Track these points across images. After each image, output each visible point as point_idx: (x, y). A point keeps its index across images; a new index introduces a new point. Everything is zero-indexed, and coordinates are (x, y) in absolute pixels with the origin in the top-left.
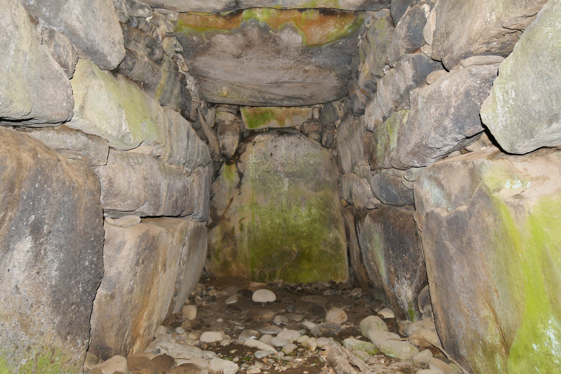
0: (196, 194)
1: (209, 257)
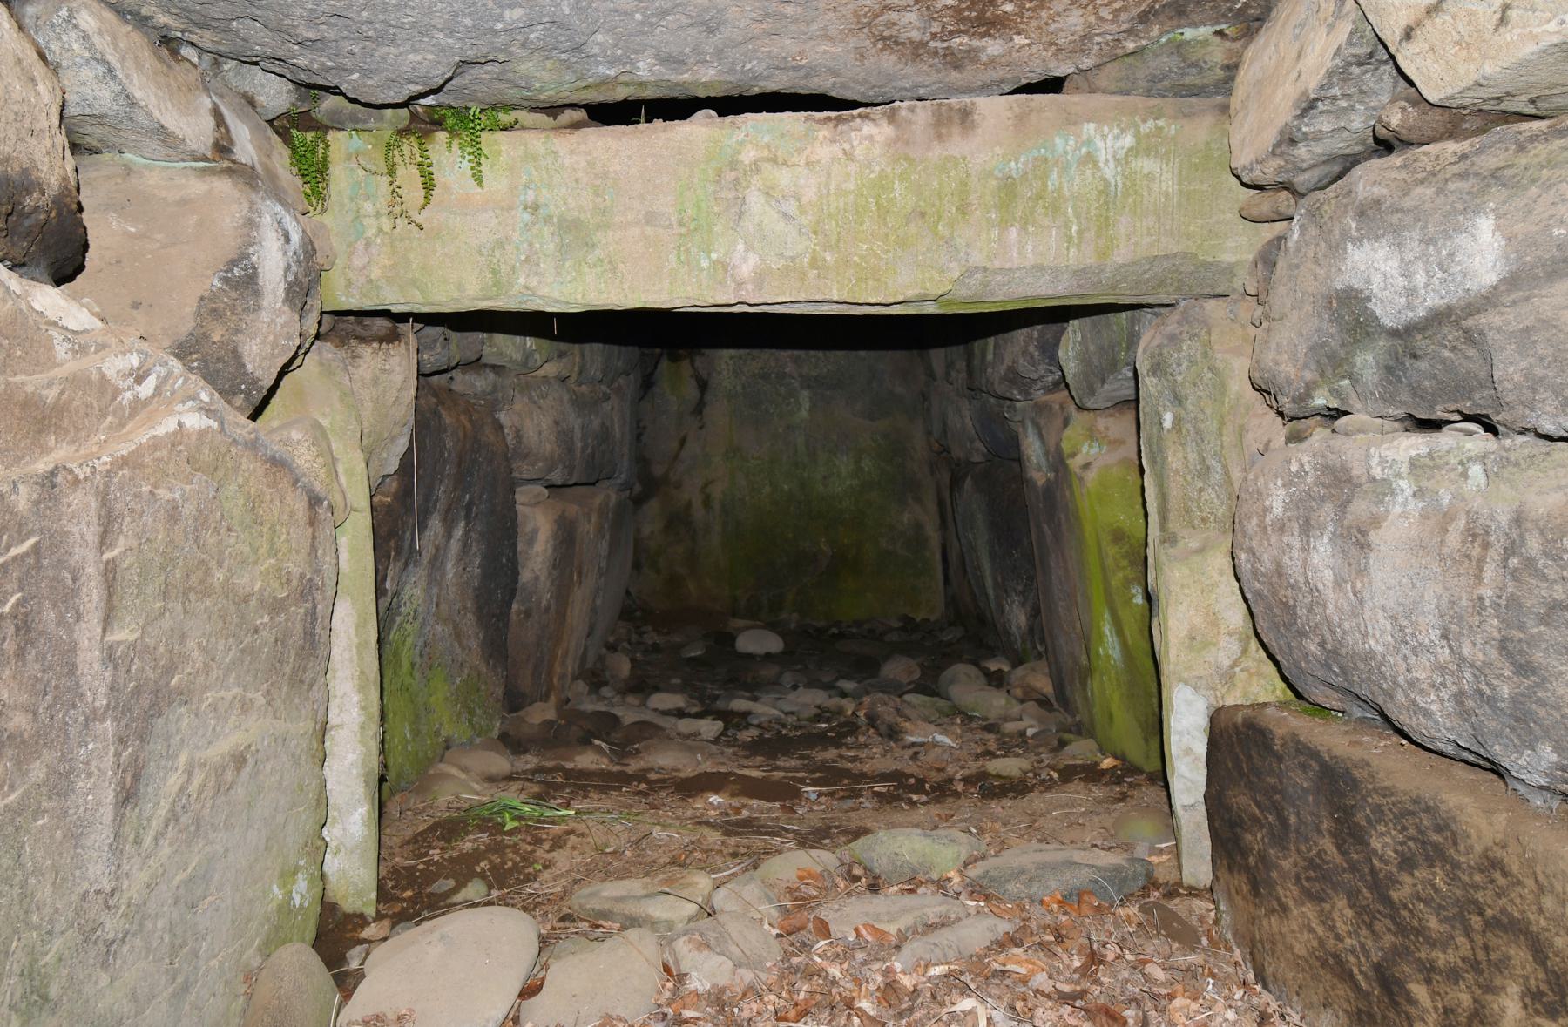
0: (618, 435)
1: (637, 566)
